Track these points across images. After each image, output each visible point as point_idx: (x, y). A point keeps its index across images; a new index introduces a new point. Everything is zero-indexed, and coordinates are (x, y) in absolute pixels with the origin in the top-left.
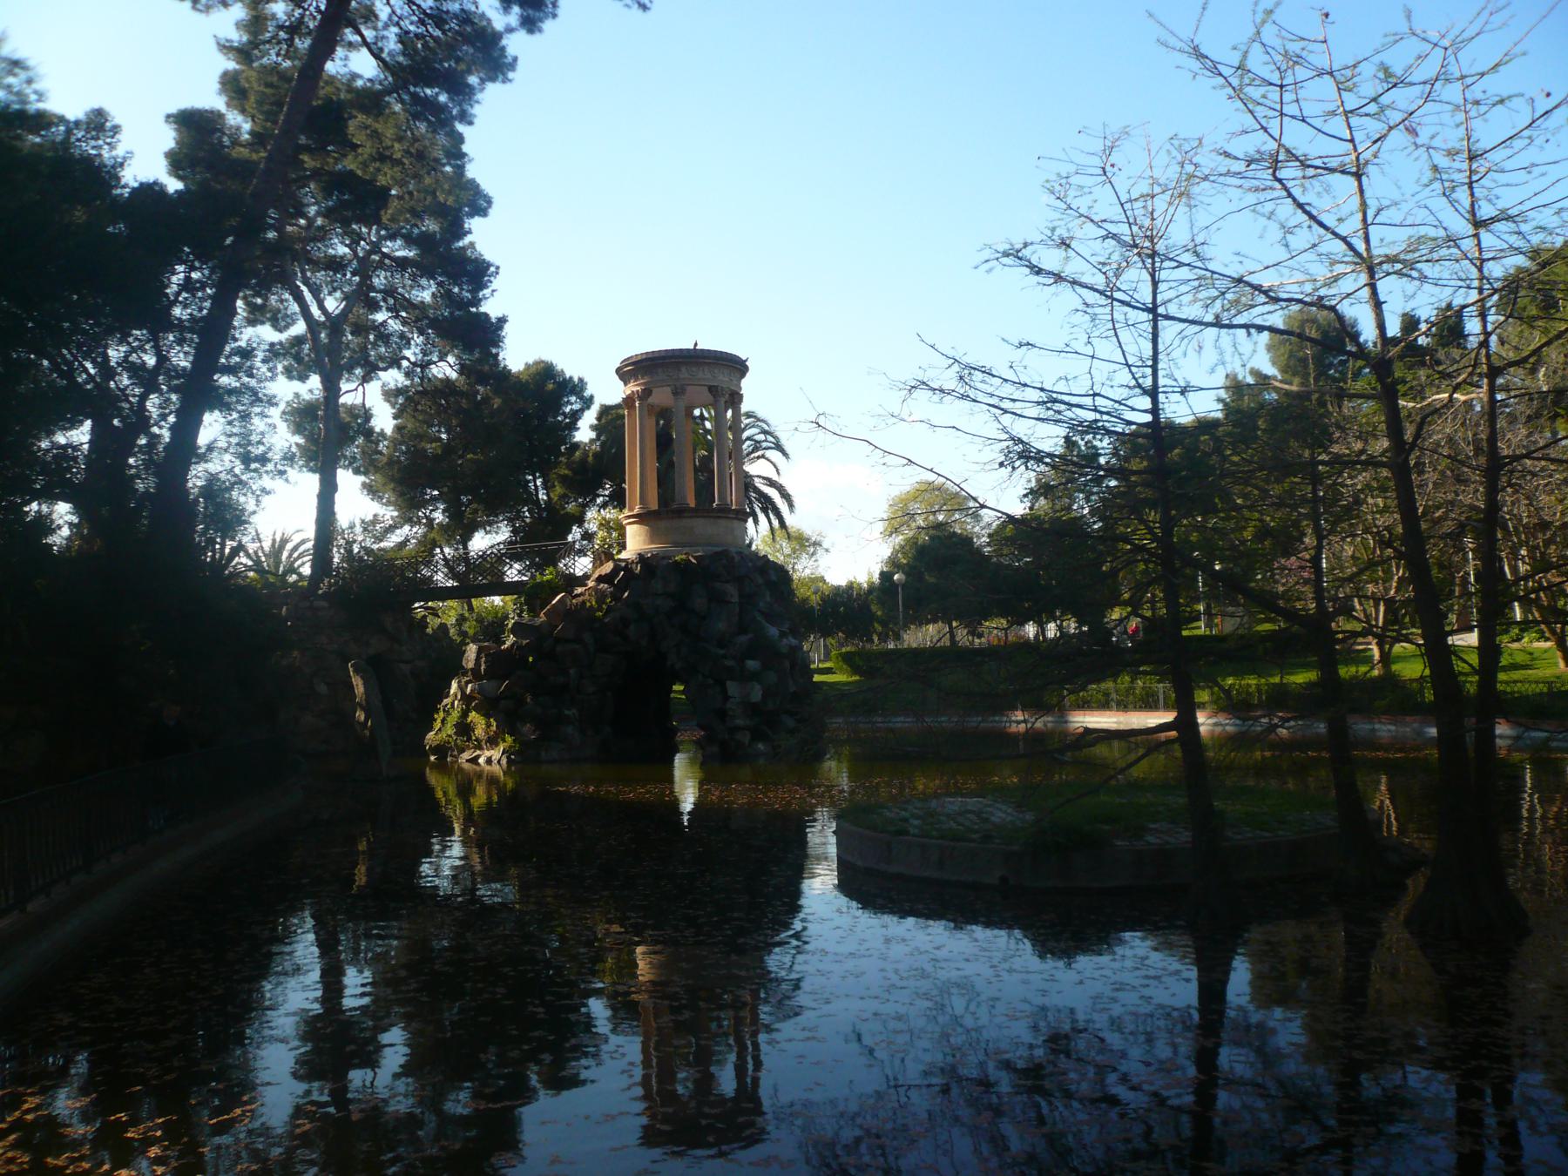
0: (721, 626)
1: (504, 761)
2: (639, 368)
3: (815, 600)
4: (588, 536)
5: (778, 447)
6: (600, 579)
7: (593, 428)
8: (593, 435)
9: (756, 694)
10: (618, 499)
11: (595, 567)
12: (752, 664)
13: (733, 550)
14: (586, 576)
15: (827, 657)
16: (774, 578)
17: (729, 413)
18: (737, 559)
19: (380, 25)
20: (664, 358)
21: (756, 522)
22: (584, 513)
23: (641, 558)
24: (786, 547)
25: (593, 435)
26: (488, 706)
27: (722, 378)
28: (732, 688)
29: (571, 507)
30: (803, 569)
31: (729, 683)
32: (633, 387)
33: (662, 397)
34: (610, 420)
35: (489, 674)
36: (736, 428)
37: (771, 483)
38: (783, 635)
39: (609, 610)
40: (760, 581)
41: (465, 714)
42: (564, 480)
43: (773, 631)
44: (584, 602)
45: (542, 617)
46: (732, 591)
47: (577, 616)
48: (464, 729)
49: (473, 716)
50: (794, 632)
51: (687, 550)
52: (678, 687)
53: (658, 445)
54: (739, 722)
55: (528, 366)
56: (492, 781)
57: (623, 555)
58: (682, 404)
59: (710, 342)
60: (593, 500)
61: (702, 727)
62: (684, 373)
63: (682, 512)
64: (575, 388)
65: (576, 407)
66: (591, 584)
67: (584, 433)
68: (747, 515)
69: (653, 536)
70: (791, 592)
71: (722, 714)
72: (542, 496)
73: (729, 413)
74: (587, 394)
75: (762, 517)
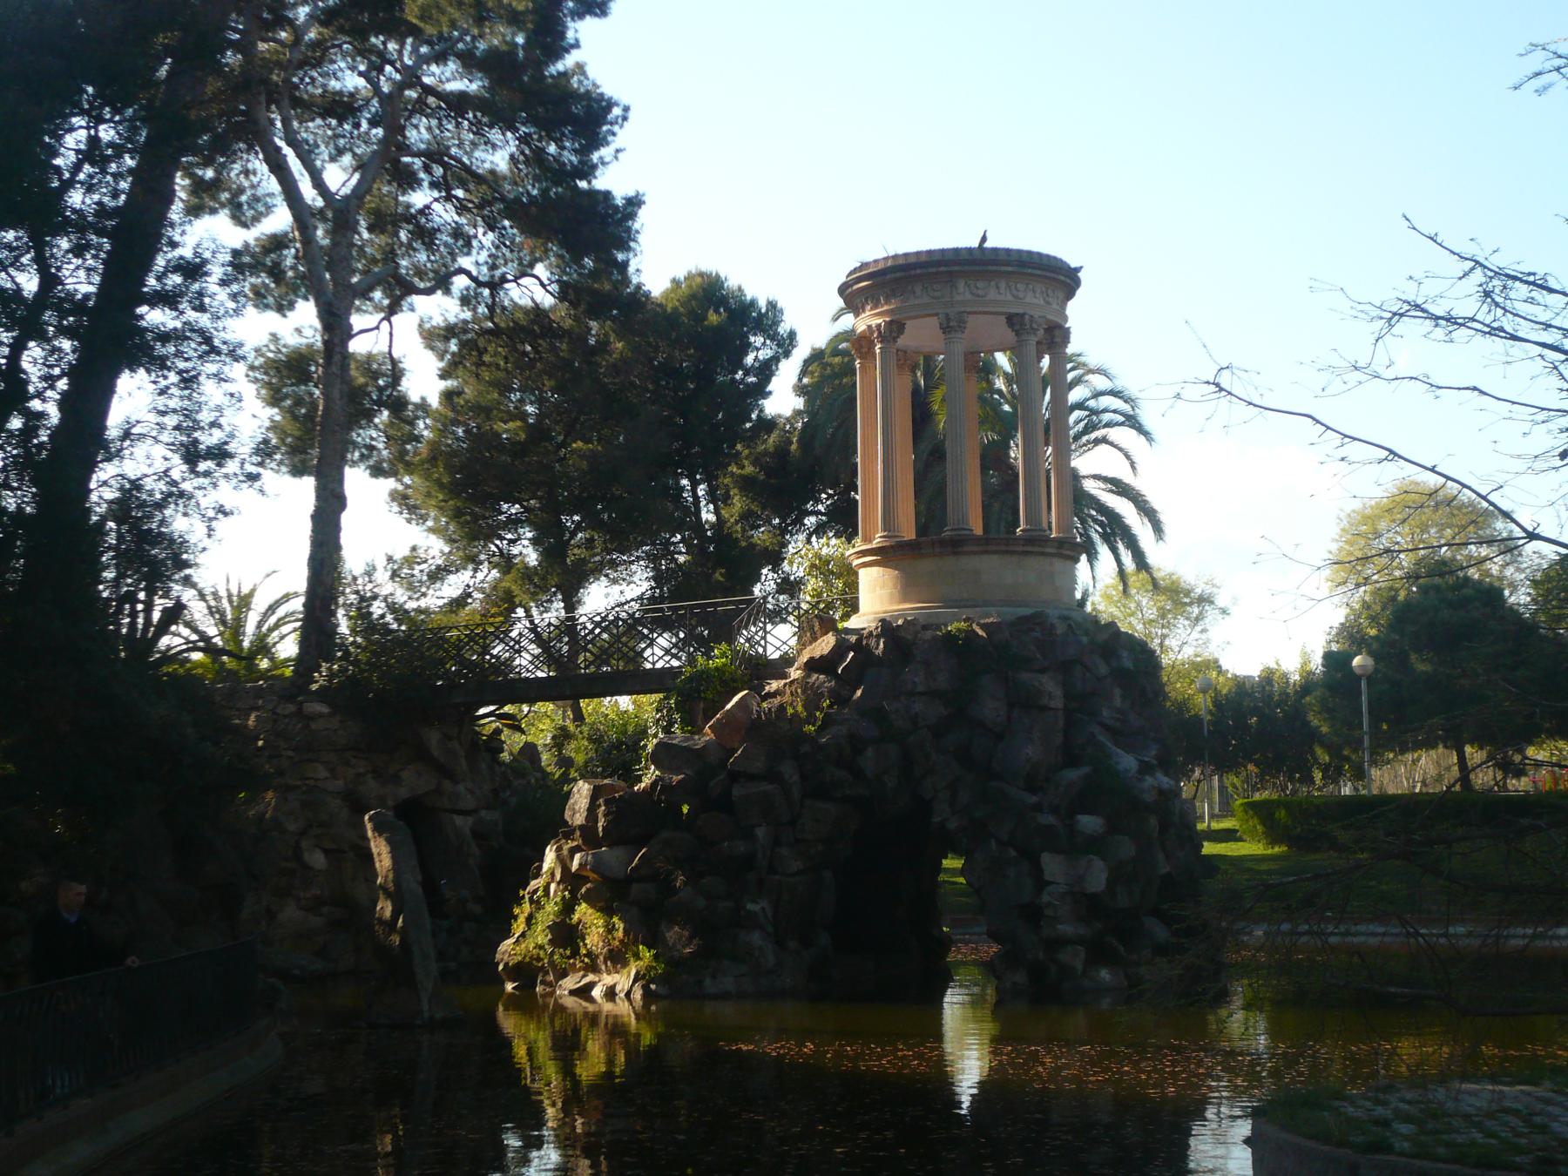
1: (638, 994)
2: (889, 283)
3: (1202, 704)
4: (789, 587)
5: (1132, 422)
6: (813, 666)
7: (800, 390)
8: (799, 403)
9: (1097, 877)
10: (843, 520)
11: (802, 644)
12: (1089, 823)
14: (787, 661)
15: (1226, 810)
16: (1128, 663)
17: (1046, 362)
18: (1060, 629)
20: (939, 263)
21: (1092, 556)
22: (784, 545)
23: (886, 627)
24: (1148, 606)
25: (799, 403)
27: (1032, 301)
28: (1053, 866)
29: (761, 535)
30: (1180, 646)
31: (1046, 858)
32: (867, 320)
33: (922, 334)
34: (831, 376)
35: (615, 836)
38: (1145, 768)
40: (1103, 669)
41: (568, 908)
42: (746, 484)
44: (782, 708)
45: (708, 735)
46: (1051, 688)
47: (771, 733)
48: (566, 934)
49: (583, 911)
54: (1066, 929)
57: (854, 622)
58: (959, 348)
60: (799, 521)
61: (994, 936)
62: (963, 292)
63: (958, 544)
64: (764, 320)
65: (765, 354)
66: (795, 673)
67: (782, 399)
69: (908, 588)
71: (1033, 914)
72: (708, 515)
73: (1046, 362)
74: (783, 329)
75: (1103, 551)
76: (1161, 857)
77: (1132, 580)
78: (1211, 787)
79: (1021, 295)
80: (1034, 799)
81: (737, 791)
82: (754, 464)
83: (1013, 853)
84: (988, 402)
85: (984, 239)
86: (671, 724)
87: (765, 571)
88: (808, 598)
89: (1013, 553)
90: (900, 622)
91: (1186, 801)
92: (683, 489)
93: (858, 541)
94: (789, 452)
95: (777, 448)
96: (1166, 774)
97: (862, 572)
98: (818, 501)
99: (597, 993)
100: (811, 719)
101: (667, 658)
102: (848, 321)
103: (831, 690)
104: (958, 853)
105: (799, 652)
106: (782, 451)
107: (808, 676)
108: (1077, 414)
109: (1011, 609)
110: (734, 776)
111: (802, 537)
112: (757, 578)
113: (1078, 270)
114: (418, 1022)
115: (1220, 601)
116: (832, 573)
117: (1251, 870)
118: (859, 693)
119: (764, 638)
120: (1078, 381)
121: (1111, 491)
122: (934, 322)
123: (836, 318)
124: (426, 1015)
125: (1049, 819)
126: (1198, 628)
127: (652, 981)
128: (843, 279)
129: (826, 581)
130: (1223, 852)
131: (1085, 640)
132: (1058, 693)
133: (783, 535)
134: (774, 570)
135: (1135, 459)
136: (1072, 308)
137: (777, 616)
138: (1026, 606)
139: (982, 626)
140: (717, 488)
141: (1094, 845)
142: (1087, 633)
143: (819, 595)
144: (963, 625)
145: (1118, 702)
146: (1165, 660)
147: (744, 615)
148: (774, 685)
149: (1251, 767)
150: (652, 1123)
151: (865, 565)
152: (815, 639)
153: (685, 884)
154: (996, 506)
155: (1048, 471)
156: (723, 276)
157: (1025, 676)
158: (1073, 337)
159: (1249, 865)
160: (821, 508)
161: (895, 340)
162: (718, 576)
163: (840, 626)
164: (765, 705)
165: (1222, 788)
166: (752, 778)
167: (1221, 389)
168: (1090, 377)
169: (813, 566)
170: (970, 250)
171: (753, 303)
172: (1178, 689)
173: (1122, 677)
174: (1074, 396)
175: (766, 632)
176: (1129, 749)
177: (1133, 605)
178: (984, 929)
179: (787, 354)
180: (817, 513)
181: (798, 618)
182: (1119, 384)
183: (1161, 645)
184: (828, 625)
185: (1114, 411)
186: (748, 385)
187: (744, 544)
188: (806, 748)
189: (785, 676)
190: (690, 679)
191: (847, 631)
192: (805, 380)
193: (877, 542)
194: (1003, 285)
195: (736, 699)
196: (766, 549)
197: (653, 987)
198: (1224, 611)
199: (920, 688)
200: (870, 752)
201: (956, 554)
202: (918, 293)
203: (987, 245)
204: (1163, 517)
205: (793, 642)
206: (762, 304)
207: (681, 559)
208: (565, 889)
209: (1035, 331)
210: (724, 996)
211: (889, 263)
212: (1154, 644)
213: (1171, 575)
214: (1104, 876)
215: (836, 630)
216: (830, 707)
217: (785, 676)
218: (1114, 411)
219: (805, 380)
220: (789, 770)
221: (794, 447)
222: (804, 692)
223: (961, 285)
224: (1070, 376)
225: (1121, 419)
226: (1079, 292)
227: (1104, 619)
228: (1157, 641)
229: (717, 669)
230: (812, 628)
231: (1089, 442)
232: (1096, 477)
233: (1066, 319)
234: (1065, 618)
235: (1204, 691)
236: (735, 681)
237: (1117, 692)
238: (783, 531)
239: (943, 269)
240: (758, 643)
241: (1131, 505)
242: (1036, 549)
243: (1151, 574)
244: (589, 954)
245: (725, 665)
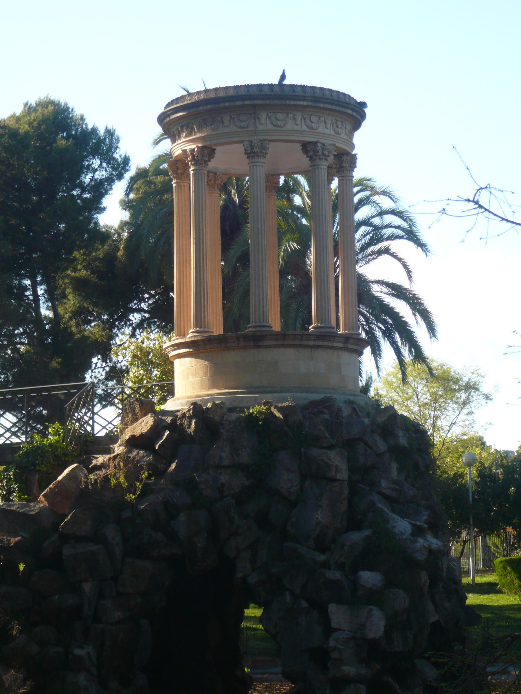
0: (320, 516)
2: (201, 113)
3: (471, 475)
4: (116, 374)
5: (411, 235)
6: (133, 443)
7: (127, 205)
8: (126, 216)
9: (376, 624)
10: (163, 316)
11: (125, 424)
12: (370, 578)
13: (339, 398)
14: (111, 438)
15: (488, 566)
16: (403, 442)
17: (335, 184)
18: (346, 411)
19: (167, 178)
20: (243, 98)
21: (376, 352)
22: (112, 337)
23: (197, 410)
24: (423, 391)
25: (126, 216)
27: (324, 131)
28: (338, 615)
29: (92, 329)
30: (449, 426)
31: (332, 608)
32: (183, 146)
33: (230, 158)
34: (153, 193)
36: (344, 205)
37: (398, 291)
38: (418, 532)
39: (146, 491)
40: (382, 447)
42: (80, 285)
43: (402, 526)
44: (106, 479)
45: (42, 502)
46: (338, 462)
47: (98, 501)
50: (435, 527)
51: (269, 397)
52: (253, 612)
53: (223, 233)
54: (349, 670)
55: (29, 109)
57: (170, 405)
58: (262, 169)
59: (303, 75)
60: (124, 318)
61: (287, 676)
62: (265, 123)
63: (259, 339)
64: (100, 145)
66: (118, 449)
67: (113, 214)
68: (363, 344)
69: (216, 376)
70: (431, 464)
71: (322, 657)
72: (45, 312)
73: (335, 184)
74: (118, 155)
75: (385, 346)
76: (431, 607)
77: (410, 369)
78: (476, 547)
79: (314, 126)
80: (322, 558)
81: (67, 551)
82: (86, 268)
83: (304, 604)
84: (288, 216)
85: (283, 77)
86: (10, 492)
87: (95, 360)
88: (130, 384)
89: (306, 347)
90: (209, 405)
91: (453, 559)
92: (26, 289)
93: (174, 335)
94: (115, 258)
95: (106, 255)
96: (436, 537)
97: (177, 363)
98: (142, 300)
100: (132, 489)
101: (8, 435)
102: (166, 145)
103: (149, 464)
104: (259, 605)
105: (122, 431)
106: (110, 258)
107: (130, 451)
108: (363, 229)
109: (304, 395)
110: (65, 538)
111: (128, 330)
112: (87, 366)
113: (363, 105)
115: (484, 388)
116: (151, 362)
117: (508, 618)
118: (173, 466)
119: (92, 418)
120: (362, 203)
121: (393, 295)
122: (240, 148)
123: (157, 142)
125: (334, 575)
126: (465, 411)
128: (162, 110)
129: (146, 370)
130: (485, 603)
131: (366, 421)
132: (343, 466)
133: (111, 329)
134: (104, 360)
135: (412, 268)
136: (358, 137)
137: (107, 399)
138: (317, 392)
139: (280, 409)
140: (56, 288)
141: (374, 597)
142: (368, 415)
143: (140, 381)
144: (263, 408)
145: (394, 474)
146: (437, 439)
147: (75, 398)
148: (101, 459)
149: (509, 529)
151: (179, 356)
152: (135, 419)
153: (20, 632)
154: (294, 306)
155: (337, 277)
156: (70, 105)
157: (315, 452)
158: (359, 163)
159: (508, 614)
160: (143, 306)
161: (206, 163)
162: (54, 364)
163: (158, 408)
164: (91, 476)
165: (486, 548)
167: (481, 207)
168: (376, 198)
169: (135, 356)
170: (271, 86)
171: (94, 130)
172: (450, 465)
173: (399, 453)
174: (362, 214)
175: (94, 414)
176: (403, 515)
177: (410, 391)
178: (279, 669)
179: (120, 177)
180: (140, 310)
181: (122, 401)
182: (402, 207)
183: (434, 425)
184: (147, 407)
185: (398, 227)
186: (84, 200)
187: (77, 336)
188: (126, 514)
189: (109, 451)
190: (27, 454)
191: (164, 413)
192: (132, 196)
193: (190, 336)
194: (299, 117)
195: (66, 471)
196: (96, 340)
198: (487, 397)
199: (226, 462)
200: (182, 517)
202: (226, 123)
203: (286, 82)
204: (435, 318)
205: (117, 422)
206: (102, 132)
207: (22, 348)
209: (326, 157)
211: (202, 97)
212: (428, 426)
213: (442, 366)
214: (382, 623)
215: (154, 412)
216: (148, 478)
217: (109, 451)
218: (398, 227)
219: (132, 196)
220: (111, 532)
221: (121, 253)
222: (125, 465)
223: (263, 116)
224: (356, 199)
225: (402, 233)
226: (364, 124)
227: (385, 402)
228: (430, 421)
229: (50, 445)
230: (133, 410)
231: (373, 253)
232: (378, 282)
233: (353, 146)
234: (350, 403)
235: (469, 464)
236: (66, 455)
237: (394, 466)
238: (110, 326)
239: (247, 102)
240: (87, 422)
241: (408, 307)
242: (326, 344)
243: (428, 365)
245: (57, 442)
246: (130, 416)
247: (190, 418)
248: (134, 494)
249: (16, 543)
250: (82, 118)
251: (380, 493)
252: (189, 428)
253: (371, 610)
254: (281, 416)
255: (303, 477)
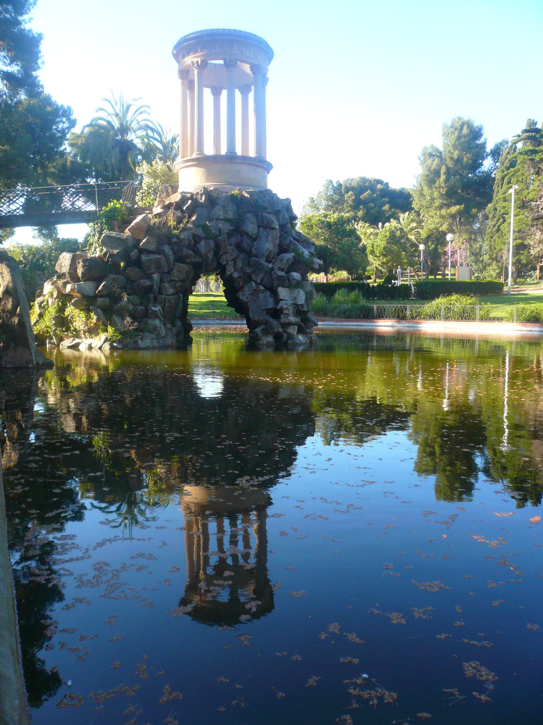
1: (107, 347)
18: (86, 268)
26: (88, 303)
28: (283, 292)
31: (280, 289)
35: (86, 277)
41: (61, 309)
48: (63, 322)
49: (70, 310)
54: (292, 319)
56: (92, 365)
65: (66, 125)
74: (72, 117)
81: (144, 258)
83: (262, 288)
99: (83, 348)
110: (142, 251)
114: (31, 366)
124: (35, 362)
127: (114, 342)
139: (248, 193)
150: (528, 488)
166: (149, 252)
188: (175, 240)
193: (194, 156)
197: (115, 344)
199: (221, 217)
200: (202, 243)
201: (231, 163)
206: (66, 107)
208: (59, 301)
210: (147, 348)
220: (167, 249)
244: (75, 330)
246: (165, 194)
247: (202, 195)
248: (178, 230)
249: (117, 253)
250: (56, 102)
251: (292, 236)
252: (201, 199)
253: (299, 291)
254: (249, 196)
255: (259, 227)
